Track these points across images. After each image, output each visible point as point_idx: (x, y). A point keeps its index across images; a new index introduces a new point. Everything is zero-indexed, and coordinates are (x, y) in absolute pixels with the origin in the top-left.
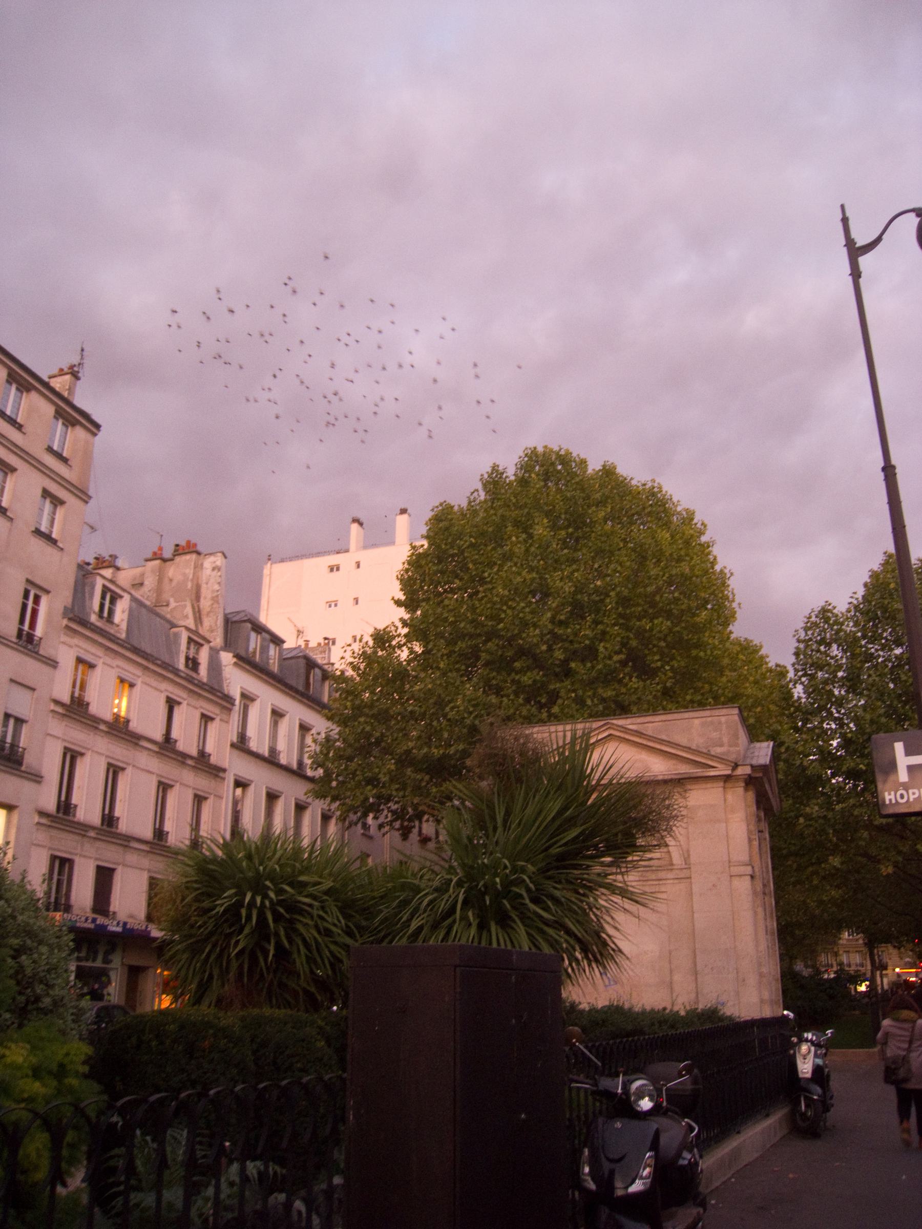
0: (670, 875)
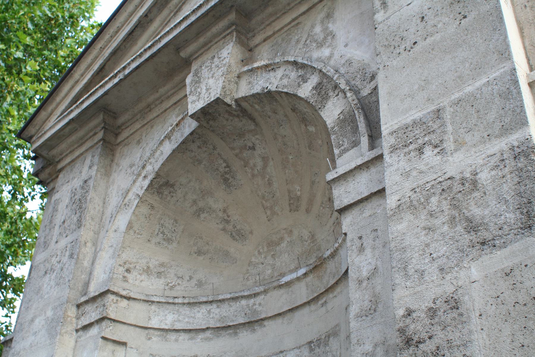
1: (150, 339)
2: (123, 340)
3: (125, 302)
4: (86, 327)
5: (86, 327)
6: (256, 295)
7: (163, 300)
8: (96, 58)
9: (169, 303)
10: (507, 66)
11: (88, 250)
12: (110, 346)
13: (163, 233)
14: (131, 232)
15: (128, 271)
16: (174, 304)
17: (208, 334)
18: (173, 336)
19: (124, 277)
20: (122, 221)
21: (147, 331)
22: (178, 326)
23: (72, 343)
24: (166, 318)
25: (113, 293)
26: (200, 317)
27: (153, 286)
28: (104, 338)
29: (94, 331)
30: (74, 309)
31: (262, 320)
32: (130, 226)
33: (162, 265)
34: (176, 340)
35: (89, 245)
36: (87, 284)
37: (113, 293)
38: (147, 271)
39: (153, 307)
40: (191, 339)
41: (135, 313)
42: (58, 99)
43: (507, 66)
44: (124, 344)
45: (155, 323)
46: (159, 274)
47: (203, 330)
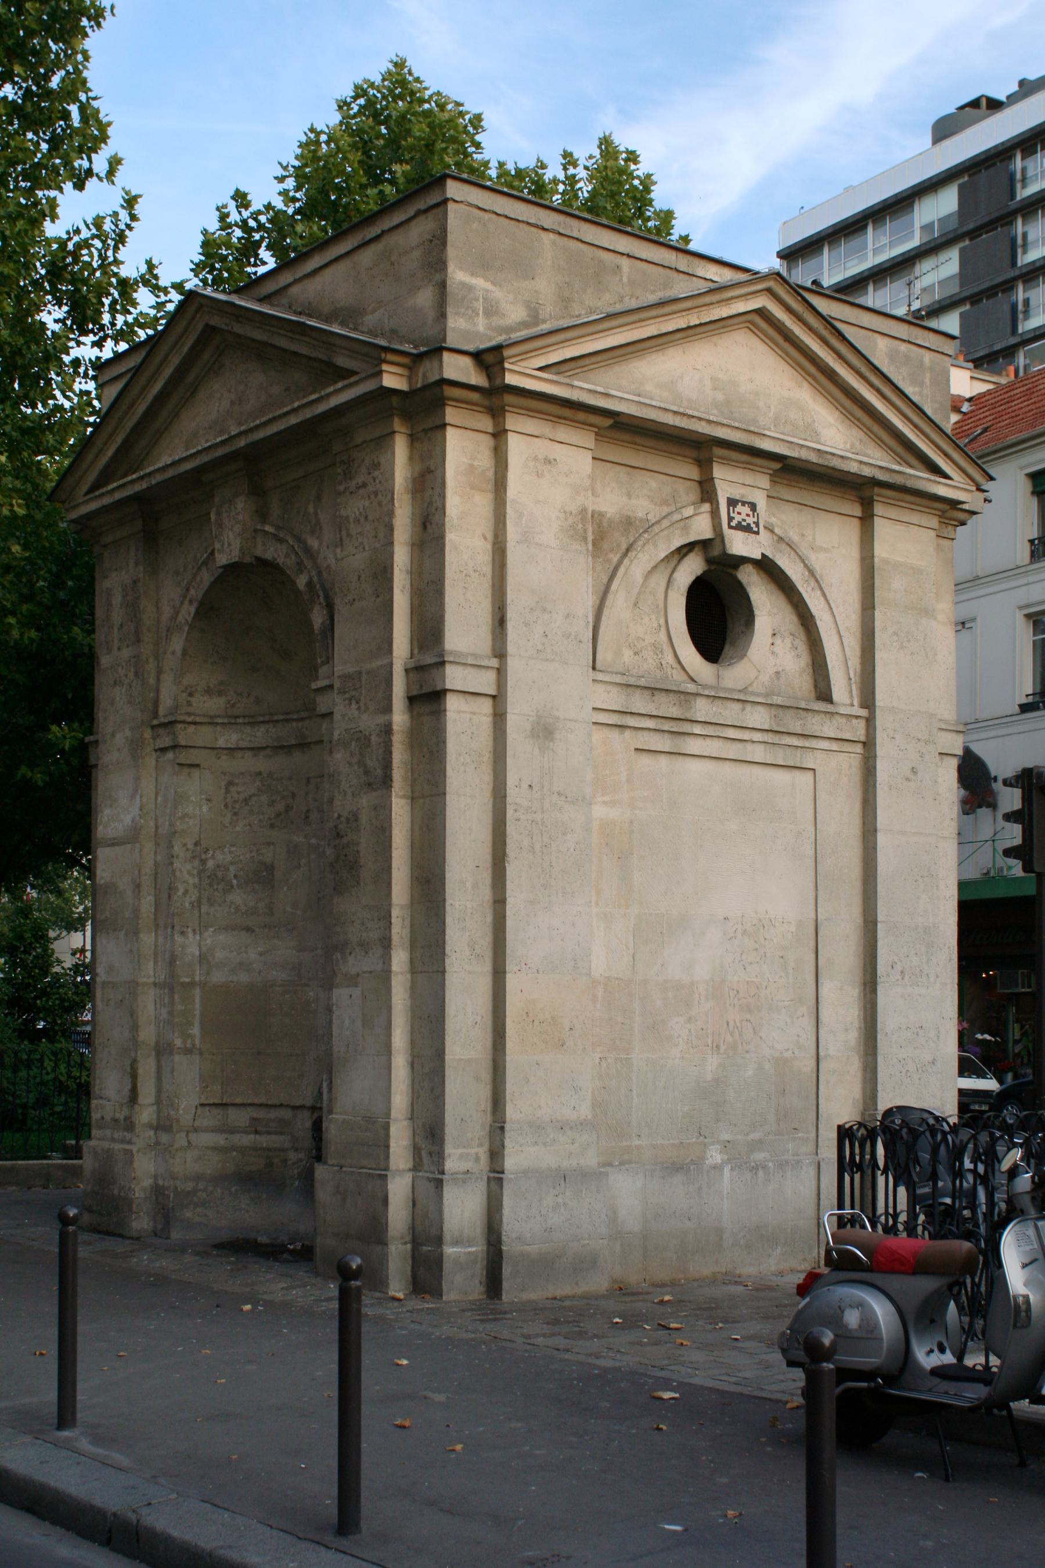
0: (829, 729)
1: (219, 758)
2: (197, 762)
3: (192, 728)
4: (163, 750)
5: (163, 750)
6: (302, 719)
7: (226, 721)
8: (115, 430)
9: (230, 723)
10: (381, 719)
11: (151, 666)
12: (186, 770)
13: (217, 652)
14: (188, 658)
15: (191, 695)
16: (236, 724)
17: (268, 752)
18: (239, 754)
19: (188, 702)
20: (177, 644)
21: (216, 751)
22: (243, 744)
23: (154, 763)
24: (229, 738)
25: (180, 722)
26: (260, 735)
27: (214, 705)
28: (179, 764)
29: (170, 755)
30: (149, 730)
31: (310, 743)
32: (185, 653)
33: (222, 683)
34: (243, 758)
35: (151, 660)
36: (156, 702)
37: (180, 722)
38: (208, 691)
39: (218, 728)
40: (255, 755)
41: (203, 735)
42: (84, 465)
43: (381, 719)
44: (197, 766)
45: (221, 743)
46: (220, 694)
47: (264, 748)
